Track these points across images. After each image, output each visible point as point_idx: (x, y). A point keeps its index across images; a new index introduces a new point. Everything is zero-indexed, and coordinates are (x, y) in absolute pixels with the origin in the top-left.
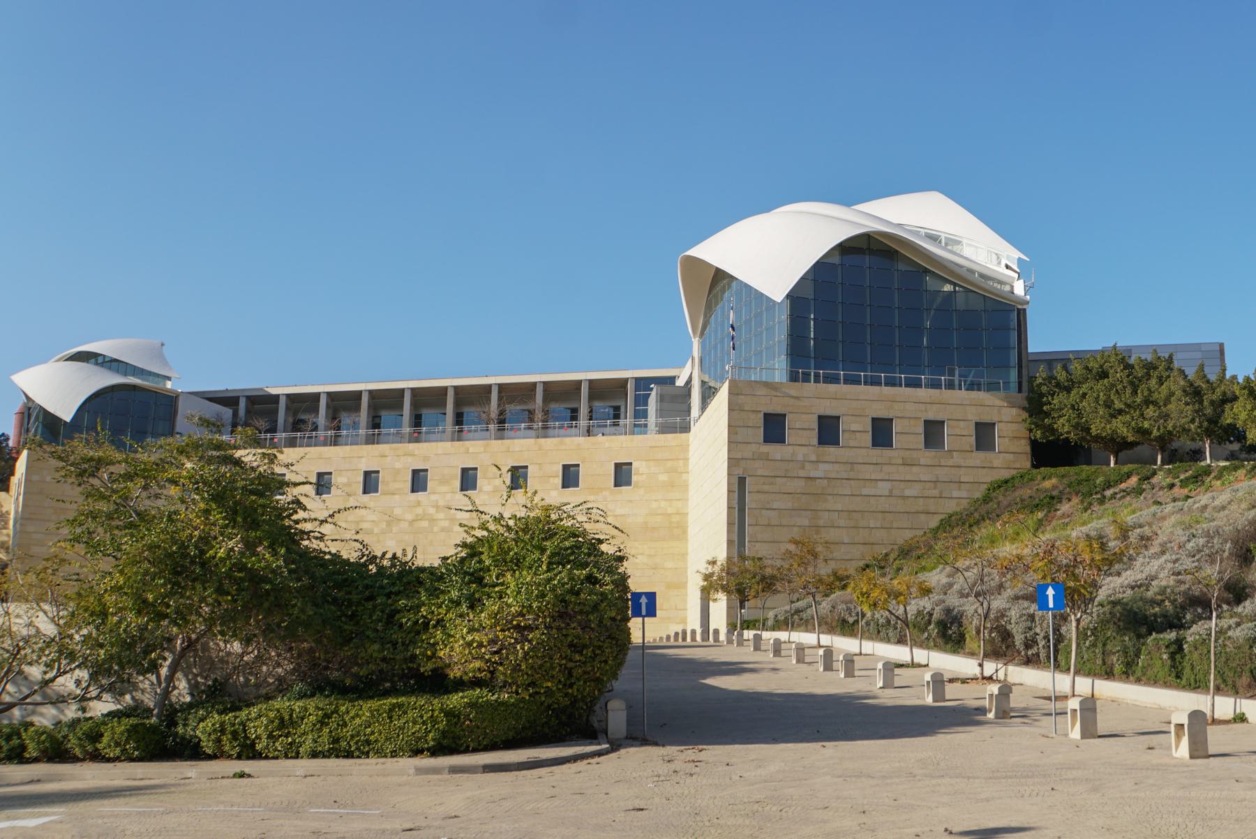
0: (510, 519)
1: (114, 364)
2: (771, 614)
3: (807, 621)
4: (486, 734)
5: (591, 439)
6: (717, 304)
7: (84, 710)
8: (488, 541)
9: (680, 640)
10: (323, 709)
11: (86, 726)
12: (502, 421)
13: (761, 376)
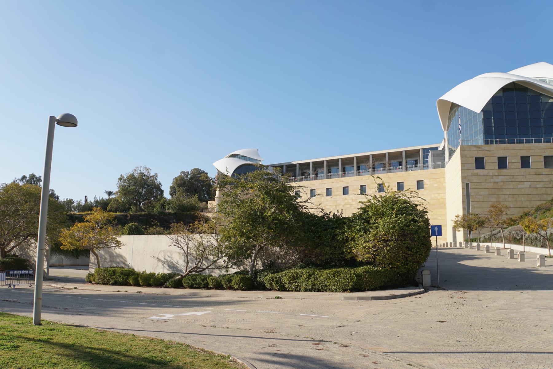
0: (379, 197)
1: (243, 157)
2: (482, 236)
3: (498, 238)
4: (372, 284)
5: (407, 172)
6: (453, 117)
7: (227, 271)
8: (371, 206)
9: (446, 246)
10: (309, 273)
11: (227, 277)
12: (374, 168)
13: (473, 143)
